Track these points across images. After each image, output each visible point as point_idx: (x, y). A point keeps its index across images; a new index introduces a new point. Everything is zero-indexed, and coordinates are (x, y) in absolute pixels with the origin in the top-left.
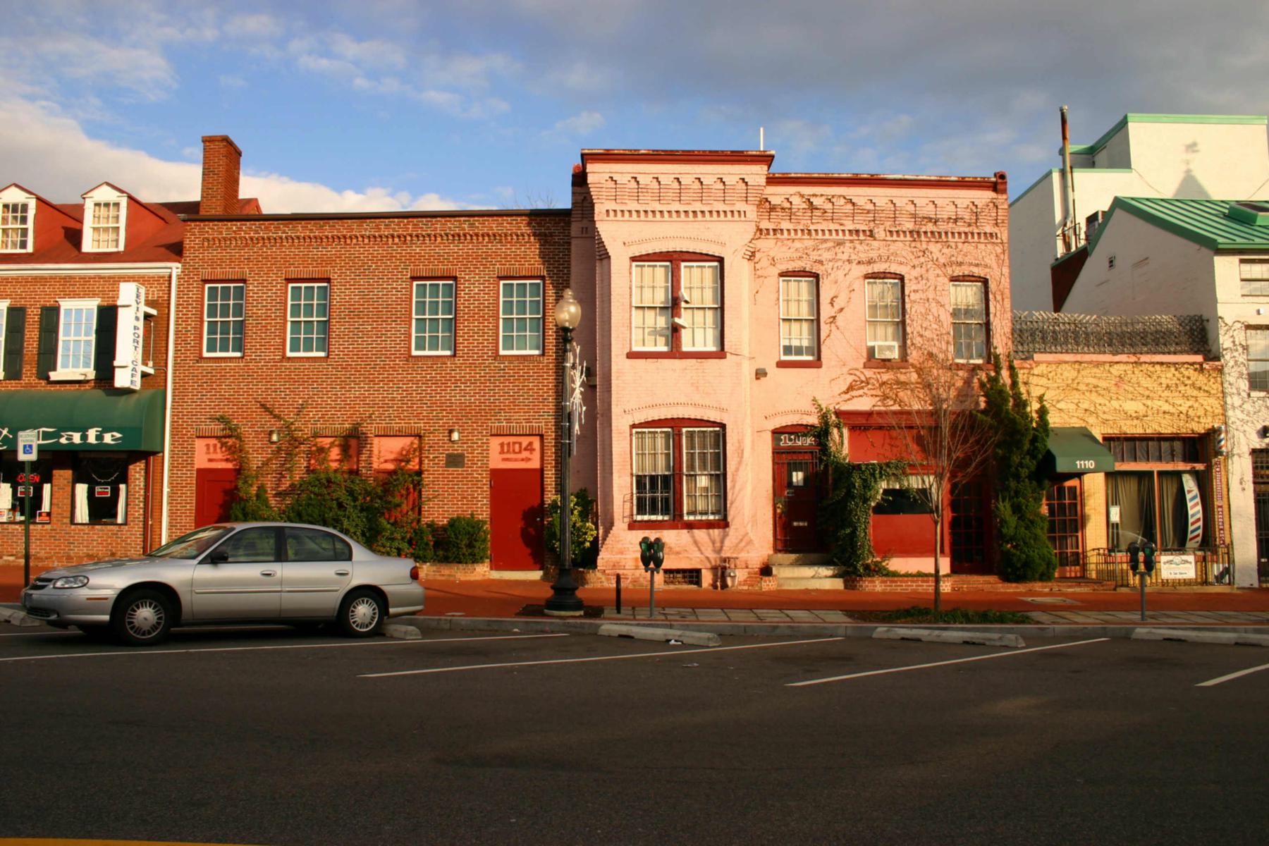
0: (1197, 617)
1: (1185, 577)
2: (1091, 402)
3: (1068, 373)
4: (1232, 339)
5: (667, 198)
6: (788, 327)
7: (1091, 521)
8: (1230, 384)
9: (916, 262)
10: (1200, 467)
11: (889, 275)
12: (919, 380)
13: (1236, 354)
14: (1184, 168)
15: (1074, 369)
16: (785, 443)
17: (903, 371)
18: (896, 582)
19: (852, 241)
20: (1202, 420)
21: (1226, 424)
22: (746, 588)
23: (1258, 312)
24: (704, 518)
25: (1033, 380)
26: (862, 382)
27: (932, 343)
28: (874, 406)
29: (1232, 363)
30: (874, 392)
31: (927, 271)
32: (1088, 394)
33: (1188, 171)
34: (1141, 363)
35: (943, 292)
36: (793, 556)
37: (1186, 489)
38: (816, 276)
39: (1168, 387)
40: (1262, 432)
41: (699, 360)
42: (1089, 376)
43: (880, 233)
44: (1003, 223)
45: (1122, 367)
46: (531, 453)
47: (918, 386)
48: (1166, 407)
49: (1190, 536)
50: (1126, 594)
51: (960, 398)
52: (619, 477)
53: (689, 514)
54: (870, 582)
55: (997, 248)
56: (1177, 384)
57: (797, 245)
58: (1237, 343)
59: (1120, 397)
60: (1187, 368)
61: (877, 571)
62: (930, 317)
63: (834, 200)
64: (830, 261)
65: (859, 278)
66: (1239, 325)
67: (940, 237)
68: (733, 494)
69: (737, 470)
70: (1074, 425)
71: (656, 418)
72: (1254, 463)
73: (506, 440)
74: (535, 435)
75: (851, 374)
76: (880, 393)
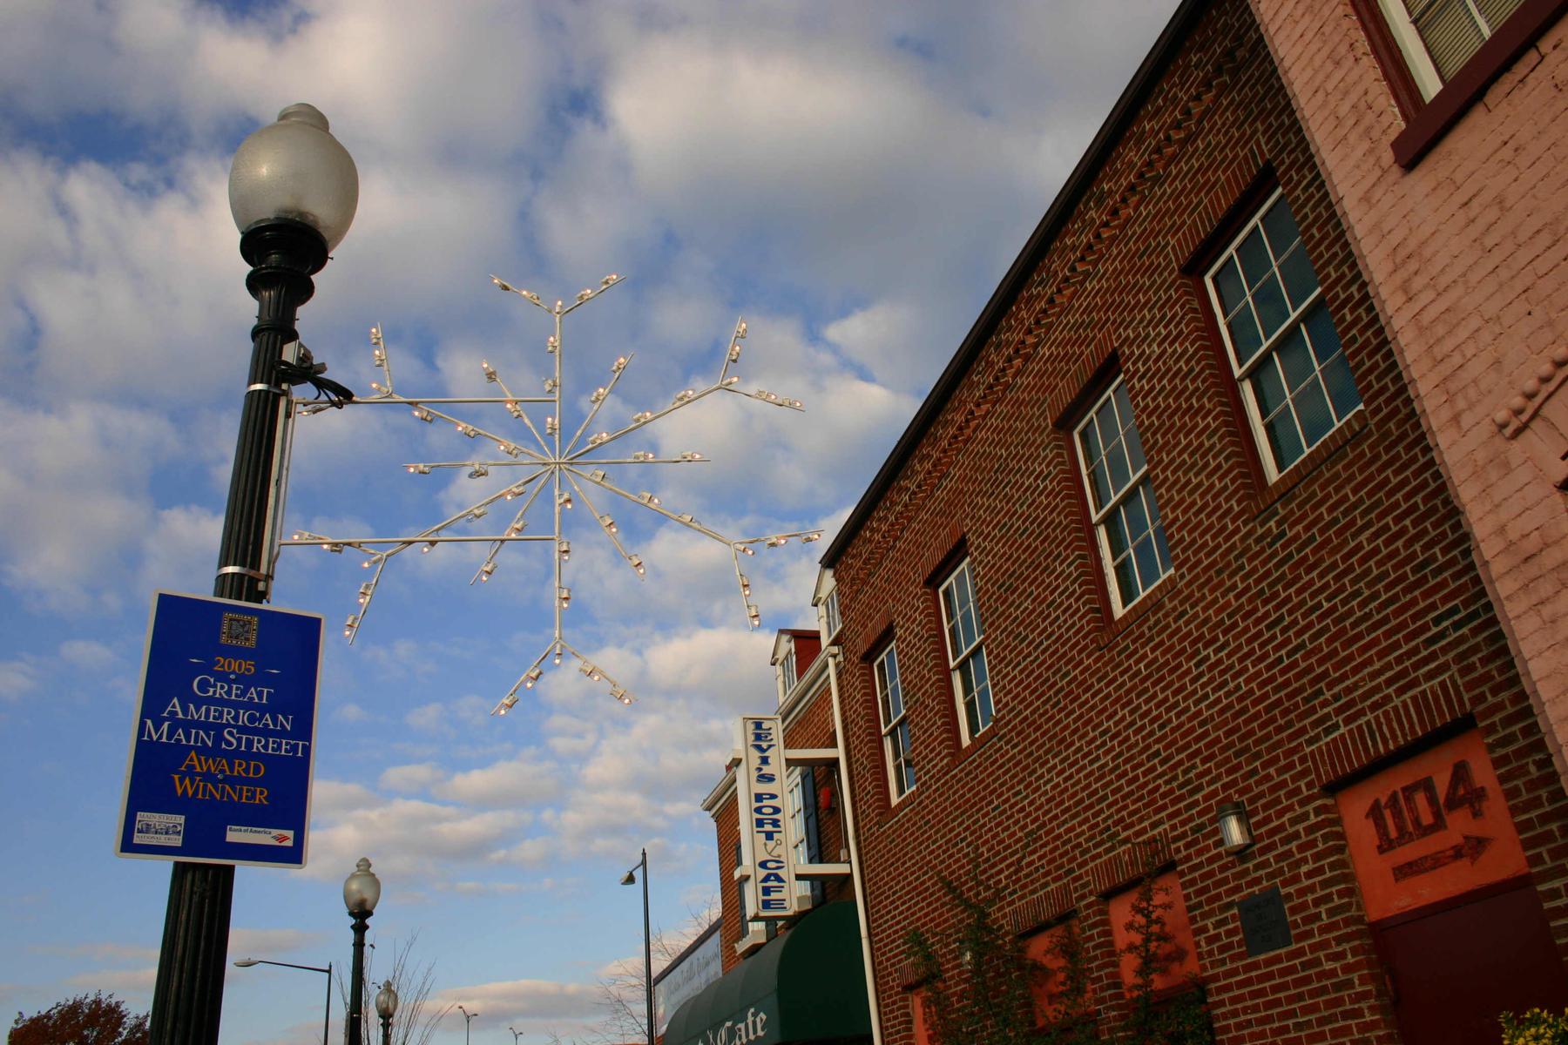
46: (1476, 814)
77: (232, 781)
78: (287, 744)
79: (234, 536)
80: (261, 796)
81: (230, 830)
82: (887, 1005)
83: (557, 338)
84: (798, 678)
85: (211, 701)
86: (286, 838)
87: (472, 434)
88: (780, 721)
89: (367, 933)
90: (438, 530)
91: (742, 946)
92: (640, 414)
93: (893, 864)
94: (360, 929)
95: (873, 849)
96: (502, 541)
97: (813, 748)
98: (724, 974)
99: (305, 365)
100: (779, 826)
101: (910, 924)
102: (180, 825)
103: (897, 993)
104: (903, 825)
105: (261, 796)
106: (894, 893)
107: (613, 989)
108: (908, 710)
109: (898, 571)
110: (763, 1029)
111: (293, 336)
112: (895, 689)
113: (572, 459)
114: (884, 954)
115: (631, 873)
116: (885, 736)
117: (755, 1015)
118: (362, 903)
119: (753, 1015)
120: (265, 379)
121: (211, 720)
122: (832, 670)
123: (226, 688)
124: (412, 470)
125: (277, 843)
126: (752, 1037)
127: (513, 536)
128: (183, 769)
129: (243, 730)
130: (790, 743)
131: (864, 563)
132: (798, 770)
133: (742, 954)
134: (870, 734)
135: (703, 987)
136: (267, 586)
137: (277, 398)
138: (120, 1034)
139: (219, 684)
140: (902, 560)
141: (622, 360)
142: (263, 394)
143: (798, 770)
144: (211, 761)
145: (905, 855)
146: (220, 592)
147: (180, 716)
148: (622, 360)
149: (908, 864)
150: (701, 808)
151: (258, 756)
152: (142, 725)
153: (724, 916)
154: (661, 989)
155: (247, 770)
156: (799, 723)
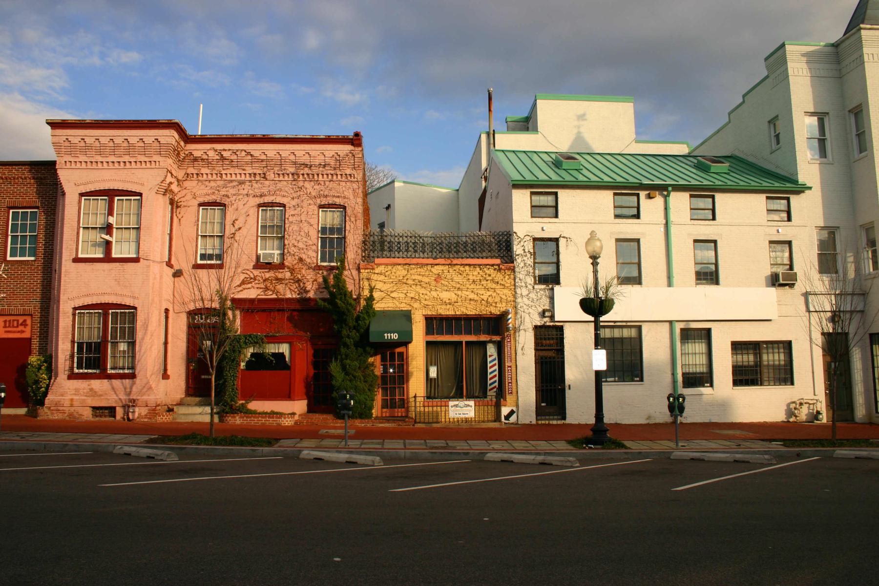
0: (436, 445)
1: (467, 416)
2: (417, 292)
3: (401, 271)
4: (523, 248)
5: (105, 153)
6: (213, 241)
7: (413, 376)
8: (520, 279)
9: (295, 195)
10: (497, 338)
11: (275, 205)
12: (292, 277)
13: (525, 258)
14: (575, 131)
15: (405, 269)
16: (198, 321)
17: (281, 271)
18: (251, 417)
19: (250, 181)
20: (498, 305)
21: (516, 308)
22: (146, 420)
23: (543, 230)
24: (121, 371)
25: (375, 277)
26: (251, 278)
27: (303, 251)
28: (259, 295)
29: (522, 265)
30: (258, 286)
31: (302, 201)
32: (414, 287)
33: (579, 133)
34: (455, 265)
35: (313, 216)
36: (198, 399)
37: (489, 353)
38: (224, 205)
39: (474, 281)
40: (542, 314)
41: (121, 264)
42: (415, 274)
43: (271, 175)
44: (359, 167)
45: (441, 268)
46: (25, 327)
47: (291, 281)
48: (472, 296)
49: (489, 388)
50: (423, 428)
51: (321, 290)
52: (63, 343)
53: (112, 369)
54: (232, 417)
55: (354, 184)
56: (480, 280)
57: (213, 184)
58: (527, 251)
59: (437, 289)
60: (489, 268)
61: (244, 411)
62: (302, 233)
63: (237, 153)
64: (234, 195)
65: (253, 207)
66: (528, 238)
67: (313, 177)
68: (140, 355)
69: (143, 339)
70: (403, 309)
71: (90, 303)
72: (536, 335)
73: (8, 318)
74: (27, 315)
75: (244, 273)
76: (263, 286)
94: (595, 264)
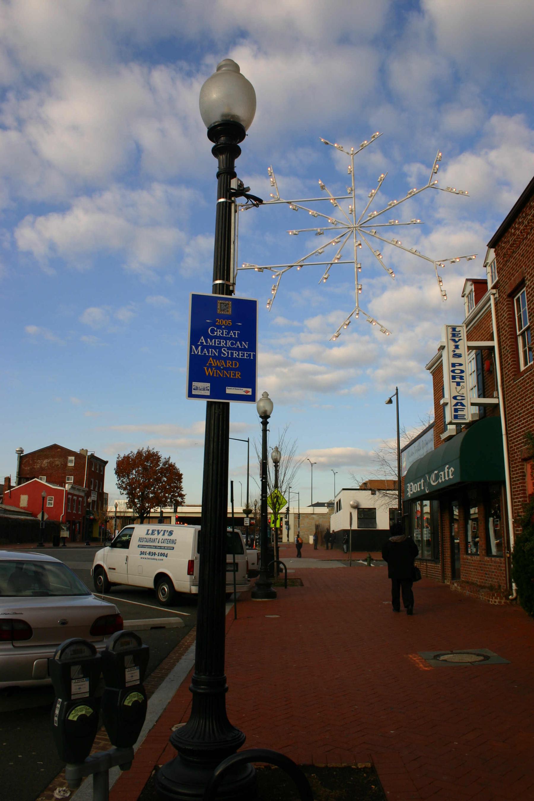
77: (227, 369)
78: (246, 354)
79: (219, 267)
80: (238, 375)
81: (227, 388)
82: (513, 467)
83: (352, 166)
84: (476, 304)
85: (216, 337)
86: (249, 392)
87: (316, 215)
88: (465, 327)
89: (268, 425)
90: (303, 260)
91: (444, 436)
92: (391, 202)
93: (520, 400)
94: (265, 423)
95: (510, 392)
96: (332, 264)
97: (482, 341)
98: (435, 449)
99: (241, 188)
100: (463, 379)
101: (527, 429)
102: (209, 387)
103: (519, 462)
104: (526, 380)
105: (238, 375)
106: (520, 414)
107: (381, 454)
108: (531, 323)
109: (528, 251)
110: (452, 475)
111: (234, 175)
112: (525, 312)
113: (361, 225)
114: (513, 443)
115: (390, 399)
116: (519, 335)
117: (448, 468)
118: (265, 412)
119: (448, 468)
120: (224, 196)
121: (217, 345)
122: (492, 302)
123: (221, 332)
124: (290, 233)
125: (245, 394)
126: (447, 478)
127: (336, 261)
128: (208, 365)
129: (229, 348)
130: (469, 339)
131: (511, 246)
132: (474, 351)
133: (443, 440)
134: (511, 335)
135: (425, 454)
136: (233, 288)
137: (230, 204)
138: (159, 465)
139: (218, 330)
140: (531, 245)
141: (382, 176)
142: (224, 203)
143: (474, 351)
144: (218, 361)
145: (526, 396)
146: (215, 292)
147: (205, 344)
148: (382, 176)
149: (527, 400)
150: (425, 368)
151: (236, 359)
152: (191, 348)
153: (435, 422)
154: (404, 455)
155: (232, 365)
156: (475, 328)
